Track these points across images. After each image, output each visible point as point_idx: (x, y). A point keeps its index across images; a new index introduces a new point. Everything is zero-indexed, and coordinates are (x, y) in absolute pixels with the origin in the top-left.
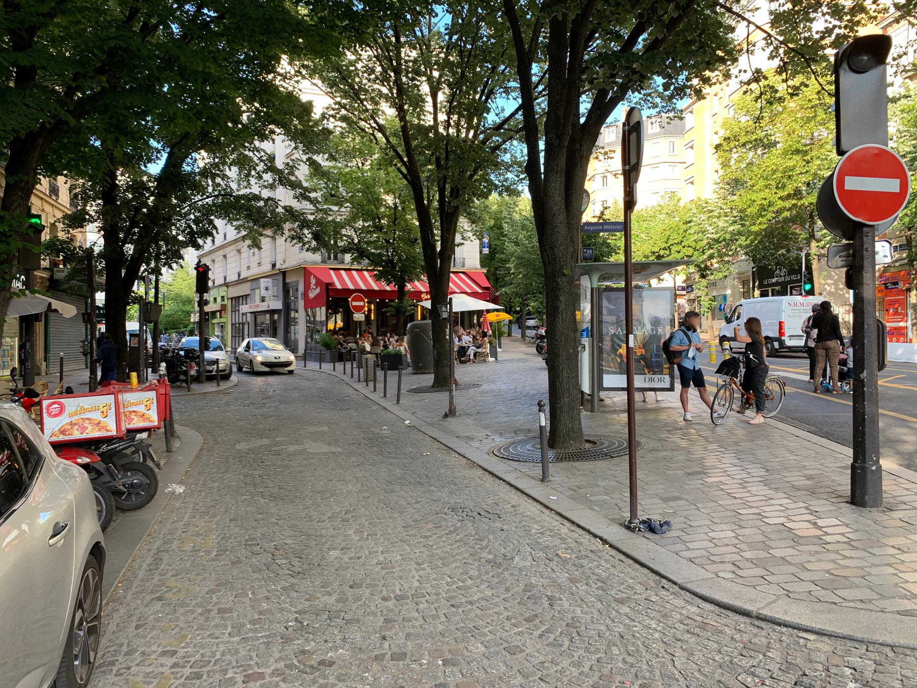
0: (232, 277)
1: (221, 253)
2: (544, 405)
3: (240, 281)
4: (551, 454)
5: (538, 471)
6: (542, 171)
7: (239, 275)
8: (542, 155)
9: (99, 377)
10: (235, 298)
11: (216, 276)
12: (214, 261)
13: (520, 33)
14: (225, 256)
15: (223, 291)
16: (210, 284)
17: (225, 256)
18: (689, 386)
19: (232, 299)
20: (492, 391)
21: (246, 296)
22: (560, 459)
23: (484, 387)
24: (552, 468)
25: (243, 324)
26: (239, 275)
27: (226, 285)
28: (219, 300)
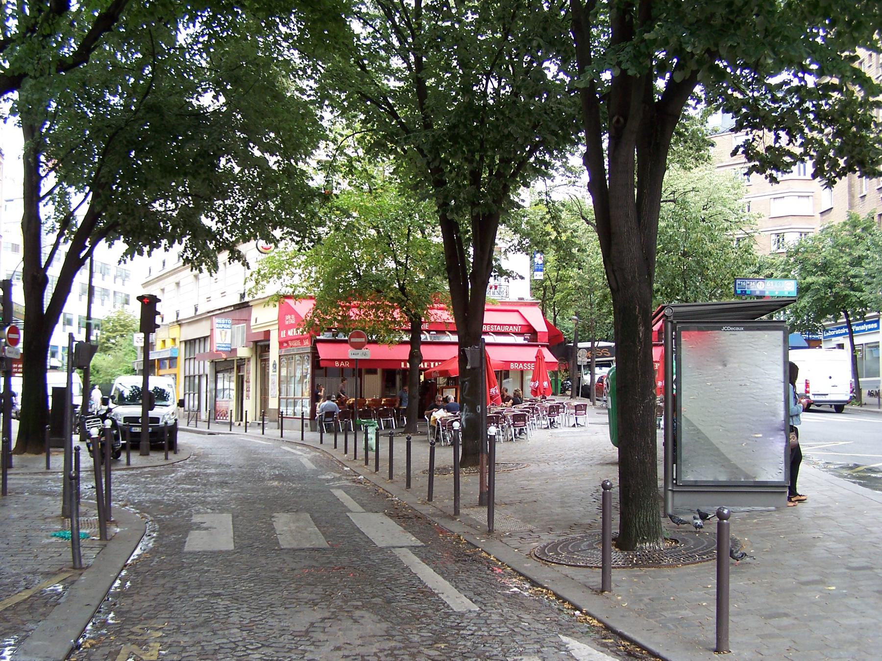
0: (187, 313)
1: (173, 279)
2: (610, 487)
3: (196, 319)
4: (616, 555)
5: (596, 579)
6: (606, 167)
7: (196, 310)
8: (50, 399)
9: (13, 445)
10: (190, 341)
11: (166, 310)
12: (163, 290)
13: (110, 490)
14: (178, 284)
15: (176, 332)
16: (158, 320)
17: (178, 284)
18: (174, 242)
19: (186, 342)
20: (543, 473)
21: (205, 338)
22: (629, 564)
23: (533, 468)
24: (616, 575)
25: (200, 376)
26: (196, 310)
27: (179, 323)
28: (169, 343)
